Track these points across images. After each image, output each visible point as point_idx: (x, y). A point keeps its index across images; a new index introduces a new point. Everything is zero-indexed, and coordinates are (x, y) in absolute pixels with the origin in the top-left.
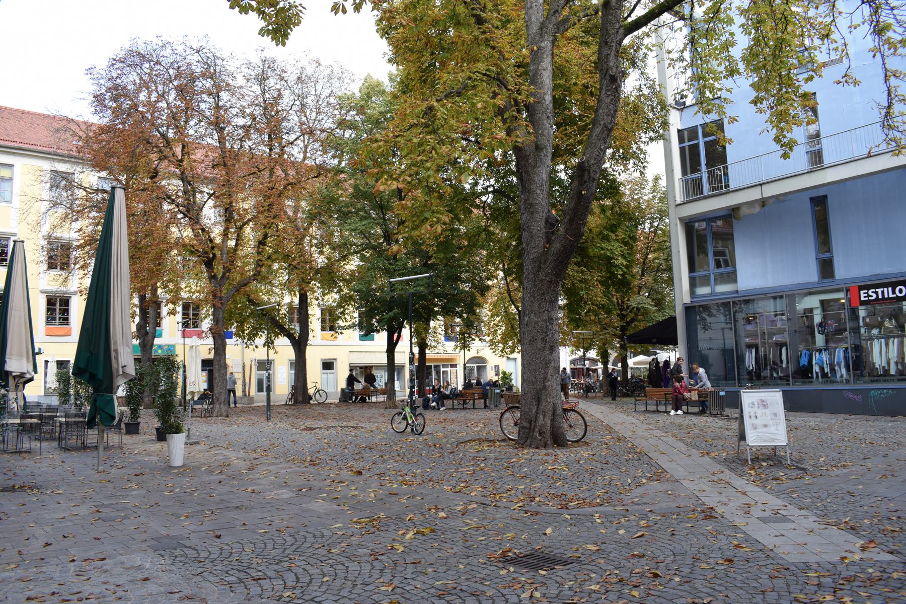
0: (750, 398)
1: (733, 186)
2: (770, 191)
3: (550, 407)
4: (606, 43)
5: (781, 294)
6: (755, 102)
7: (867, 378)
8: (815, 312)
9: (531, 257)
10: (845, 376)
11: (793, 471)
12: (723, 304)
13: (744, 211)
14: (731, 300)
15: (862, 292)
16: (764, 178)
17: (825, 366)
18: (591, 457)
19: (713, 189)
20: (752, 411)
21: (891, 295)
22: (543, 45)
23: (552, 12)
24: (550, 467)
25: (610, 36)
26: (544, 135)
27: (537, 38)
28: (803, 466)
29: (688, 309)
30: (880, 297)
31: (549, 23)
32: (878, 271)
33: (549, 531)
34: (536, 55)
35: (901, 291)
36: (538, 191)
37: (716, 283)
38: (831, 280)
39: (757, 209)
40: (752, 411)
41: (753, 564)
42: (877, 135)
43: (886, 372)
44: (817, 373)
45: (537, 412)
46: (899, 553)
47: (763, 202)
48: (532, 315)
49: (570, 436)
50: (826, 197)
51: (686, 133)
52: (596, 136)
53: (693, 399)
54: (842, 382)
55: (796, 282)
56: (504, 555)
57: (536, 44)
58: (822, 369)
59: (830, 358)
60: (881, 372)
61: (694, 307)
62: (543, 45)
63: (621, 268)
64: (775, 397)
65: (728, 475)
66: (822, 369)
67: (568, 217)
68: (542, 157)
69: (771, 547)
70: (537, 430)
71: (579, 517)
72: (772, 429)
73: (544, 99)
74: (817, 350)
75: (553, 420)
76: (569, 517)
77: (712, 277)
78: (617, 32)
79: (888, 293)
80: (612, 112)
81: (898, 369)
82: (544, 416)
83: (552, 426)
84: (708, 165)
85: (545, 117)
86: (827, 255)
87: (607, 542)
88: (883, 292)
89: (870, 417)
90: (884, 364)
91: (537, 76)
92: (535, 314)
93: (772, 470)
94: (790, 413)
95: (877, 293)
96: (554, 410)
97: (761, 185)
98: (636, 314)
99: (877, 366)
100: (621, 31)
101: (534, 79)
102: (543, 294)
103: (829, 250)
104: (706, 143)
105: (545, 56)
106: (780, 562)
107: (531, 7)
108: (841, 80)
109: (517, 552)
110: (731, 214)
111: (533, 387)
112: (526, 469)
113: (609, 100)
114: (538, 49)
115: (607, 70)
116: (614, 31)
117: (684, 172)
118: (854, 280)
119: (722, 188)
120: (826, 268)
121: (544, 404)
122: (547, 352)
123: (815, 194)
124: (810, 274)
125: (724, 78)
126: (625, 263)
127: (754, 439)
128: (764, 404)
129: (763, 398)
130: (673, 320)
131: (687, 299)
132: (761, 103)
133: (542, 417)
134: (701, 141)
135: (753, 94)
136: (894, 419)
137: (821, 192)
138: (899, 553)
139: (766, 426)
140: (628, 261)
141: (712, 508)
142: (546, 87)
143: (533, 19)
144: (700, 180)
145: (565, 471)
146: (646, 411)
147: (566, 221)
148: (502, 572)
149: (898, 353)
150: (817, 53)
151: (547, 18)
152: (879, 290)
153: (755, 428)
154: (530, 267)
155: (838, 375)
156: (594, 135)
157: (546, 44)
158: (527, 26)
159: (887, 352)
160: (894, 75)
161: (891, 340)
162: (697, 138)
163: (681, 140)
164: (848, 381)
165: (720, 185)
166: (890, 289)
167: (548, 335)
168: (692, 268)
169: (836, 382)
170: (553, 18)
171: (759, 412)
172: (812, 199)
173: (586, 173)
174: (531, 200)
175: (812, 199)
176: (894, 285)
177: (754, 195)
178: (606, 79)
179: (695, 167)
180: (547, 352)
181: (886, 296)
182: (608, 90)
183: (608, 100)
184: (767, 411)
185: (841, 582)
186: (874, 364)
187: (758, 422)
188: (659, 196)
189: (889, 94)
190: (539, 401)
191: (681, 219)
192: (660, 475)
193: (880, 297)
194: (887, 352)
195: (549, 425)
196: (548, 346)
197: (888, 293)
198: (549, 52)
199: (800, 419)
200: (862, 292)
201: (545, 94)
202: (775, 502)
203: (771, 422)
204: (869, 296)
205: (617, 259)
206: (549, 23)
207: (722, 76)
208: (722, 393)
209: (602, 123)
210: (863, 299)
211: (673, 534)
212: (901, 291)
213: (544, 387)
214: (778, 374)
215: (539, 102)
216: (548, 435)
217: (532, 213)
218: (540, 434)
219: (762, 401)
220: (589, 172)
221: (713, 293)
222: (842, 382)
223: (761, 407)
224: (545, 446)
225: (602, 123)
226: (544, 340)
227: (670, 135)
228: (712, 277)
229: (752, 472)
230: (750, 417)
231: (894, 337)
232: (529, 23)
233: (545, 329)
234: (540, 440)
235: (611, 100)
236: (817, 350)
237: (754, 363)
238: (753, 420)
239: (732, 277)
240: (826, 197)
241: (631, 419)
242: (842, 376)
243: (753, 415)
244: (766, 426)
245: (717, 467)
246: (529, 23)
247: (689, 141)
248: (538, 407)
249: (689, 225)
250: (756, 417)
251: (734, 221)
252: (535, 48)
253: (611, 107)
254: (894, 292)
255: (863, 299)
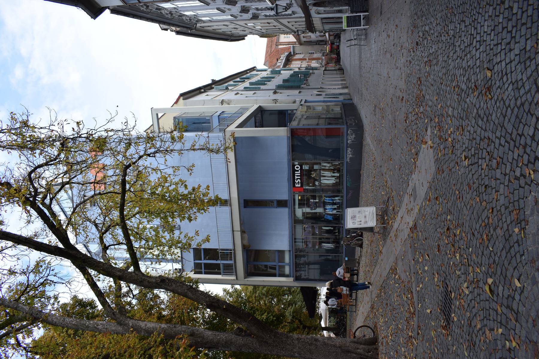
0: (350, 224)
1: (231, 247)
2: (237, 227)
3: (352, 345)
4: (141, 281)
5: (293, 227)
6: (190, 220)
7: (341, 187)
8: (304, 211)
9: (258, 347)
10: (339, 198)
11: (389, 203)
12: (296, 268)
13: (246, 242)
14: (294, 254)
15: (296, 186)
16: (230, 229)
17: (333, 207)
18: (383, 316)
19: (231, 259)
20: (357, 223)
21: (299, 172)
22: (131, 325)
23: (113, 316)
24: (390, 338)
25: (138, 279)
26: (185, 331)
27: (126, 328)
28: (387, 200)
29: (297, 279)
30: (299, 177)
31: (119, 319)
32: (286, 179)
33: (428, 311)
34: (137, 329)
35: (297, 167)
36: (219, 337)
37: (284, 262)
38: (288, 202)
39: (246, 236)
40: (357, 223)
41: (438, 186)
42: (221, 156)
43: (338, 178)
44: (337, 212)
45: (356, 354)
46: (427, 128)
47: (243, 232)
48: (295, 350)
49: (372, 336)
50: (245, 200)
51: (197, 270)
52: (193, 295)
53: (349, 276)
54: (342, 200)
55: (288, 219)
56: (444, 328)
57: (129, 329)
58: (335, 209)
59: (330, 205)
60: (338, 180)
61: (296, 276)
62: (131, 325)
63: (269, 316)
64: (350, 212)
65: (392, 234)
66: (335, 209)
67: (237, 319)
68: (198, 333)
69: (429, 184)
70: (366, 354)
71: (419, 299)
72: (367, 213)
73: (163, 328)
74: (325, 211)
75: (361, 344)
76: (420, 305)
77: (280, 264)
78: (137, 275)
79: (298, 173)
80: (181, 284)
81: (337, 172)
82: (358, 349)
83: (364, 344)
84: (217, 259)
85: (174, 329)
86: (275, 203)
87: (432, 272)
88: (297, 176)
89: (361, 186)
90: (334, 179)
91: (149, 331)
92: (294, 348)
93: (389, 214)
94: (360, 204)
95: (297, 179)
96: (354, 342)
97: (233, 231)
98: (296, 319)
99: (335, 182)
100: (137, 272)
101: (149, 332)
102: (282, 341)
103: (272, 201)
104: (205, 259)
105: (138, 324)
106: (435, 174)
107: (106, 329)
108: (190, 173)
109: (442, 321)
110: (246, 249)
111: (339, 354)
112: (392, 353)
113: (174, 285)
114: (132, 327)
115: (157, 283)
116: (136, 276)
117: (219, 274)
118: (289, 191)
119: (232, 253)
120: (282, 204)
121: (350, 348)
122: (318, 343)
123: (242, 205)
124: (284, 212)
125: (173, 235)
126: (266, 314)
127: (372, 223)
128: (354, 217)
129: (350, 218)
130: (302, 288)
131: (291, 279)
132: (192, 217)
133: (359, 350)
134: (203, 261)
135: (186, 220)
136: (362, 175)
137: (242, 202)
138: (427, 128)
139: (365, 217)
140: (265, 312)
141: (410, 229)
142: (157, 326)
143: (114, 328)
144: (224, 265)
145: (392, 328)
146: (356, 305)
147: (239, 321)
148: (455, 319)
149: (328, 171)
150: (173, 181)
151: (116, 320)
152: (296, 177)
153: (367, 222)
154: (264, 348)
155: (339, 201)
156: (192, 297)
157: (131, 322)
158: (117, 333)
159: (328, 177)
160: (194, 146)
161: (322, 174)
162: (201, 264)
163: (201, 273)
164: (342, 197)
165: (228, 254)
166: (296, 172)
167: (308, 342)
168: (274, 275)
169: (342, 202)
170: (117, 316)
171: (358, 219)
172: (245, 207)
173: (213, 304)
174: (223, 343)
175: (245, 207)
176: (294, 171)
177: (238, 235)
178: (162, 285)
179: (217, 266)
180: (318, 343)
181: (299, 174)
182: (168, 284)
183: (174, 286)
184: (357, 216)
185: (442, 140)
186: (333, 183)
187: (363, 220)
188: (228, 297)
189: (203, 149)
190: (349, 352)
191: (245, 278)
192: (394, 270)
193: (299, 177)
194: (328, 177)
195: (364, 346)
196: (314, 342)
197: (298, 173)
198: (136, 322)
199: (362, 200)
200: (296, 186)
201: (160, 327)
202: (406, 199)
203: (363, 214)
204: (298, 183)
205: (263, 318)
206: (119, 319)
207: (172, 236)
208: (346, 259)
209: (186, 291)
210: (300, 186)
211: (426, 239)
212: (297, 167)
213: (340, 347)
214: (337, 232)
215: (164, 331)
216: (370, 347)
217: (231, 343)
218: (369, 352)
219: (352, 218)
220: (213, 302)
221: (289, 265)
222: (342, 200)
223: (355, 219)
224: (377, 349)
225: (186, 291)
226: (311, 344)
227: (196, 278)
228: (280, 264)
229: (390, 222)
230: (360, 224)
231: (320, 173)
232: (115, 332)
233: (304, 343)
234: (373, 352)
235: (174, 284)
236: (325, 211)
237: (330, 245)
238: (362, 223)
239: (281, 253)
240: (245, 200)
241: (360, 313)
242: (339, 199)
243: (359, 223)
244: (365, 217)
245: (389, 241)
246: (115, 332)
247: (202, 269)
248: (352, 353)
249: (249, 274)
250: (360, 221)
251: (250, 248)
252: (131, 329)
253: (178, 284)
254: (298, 171)
255: (300, 186)
